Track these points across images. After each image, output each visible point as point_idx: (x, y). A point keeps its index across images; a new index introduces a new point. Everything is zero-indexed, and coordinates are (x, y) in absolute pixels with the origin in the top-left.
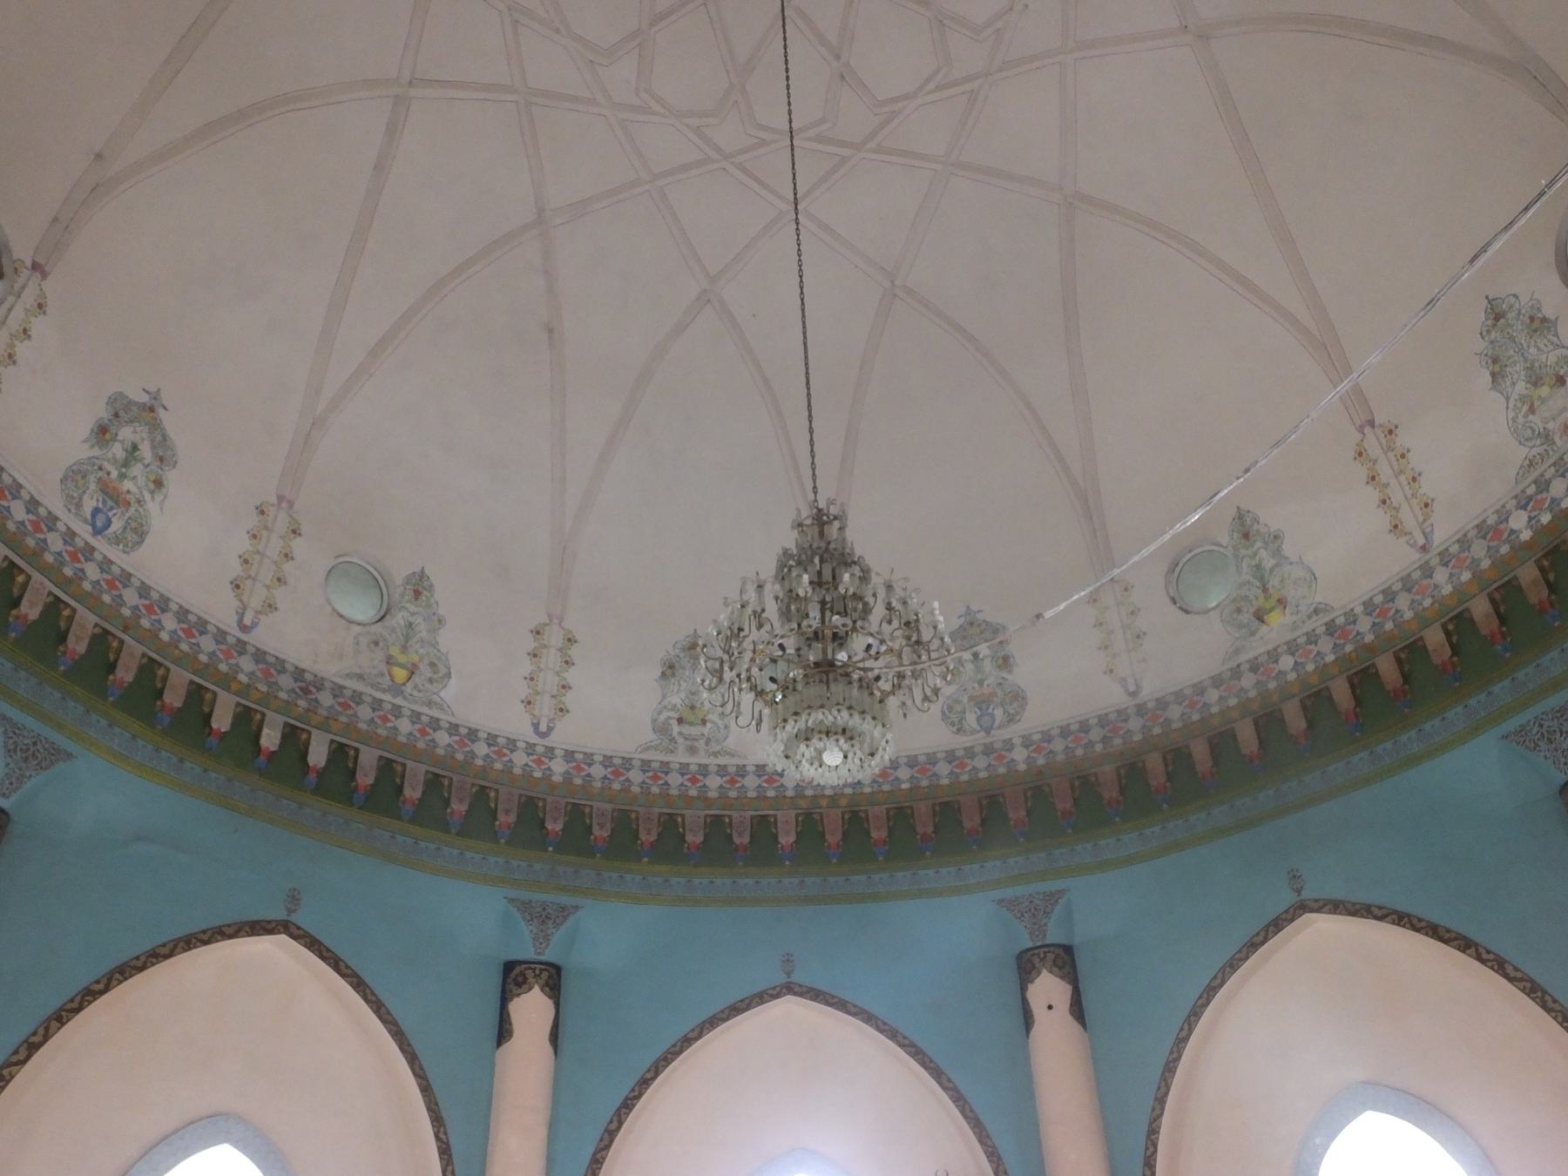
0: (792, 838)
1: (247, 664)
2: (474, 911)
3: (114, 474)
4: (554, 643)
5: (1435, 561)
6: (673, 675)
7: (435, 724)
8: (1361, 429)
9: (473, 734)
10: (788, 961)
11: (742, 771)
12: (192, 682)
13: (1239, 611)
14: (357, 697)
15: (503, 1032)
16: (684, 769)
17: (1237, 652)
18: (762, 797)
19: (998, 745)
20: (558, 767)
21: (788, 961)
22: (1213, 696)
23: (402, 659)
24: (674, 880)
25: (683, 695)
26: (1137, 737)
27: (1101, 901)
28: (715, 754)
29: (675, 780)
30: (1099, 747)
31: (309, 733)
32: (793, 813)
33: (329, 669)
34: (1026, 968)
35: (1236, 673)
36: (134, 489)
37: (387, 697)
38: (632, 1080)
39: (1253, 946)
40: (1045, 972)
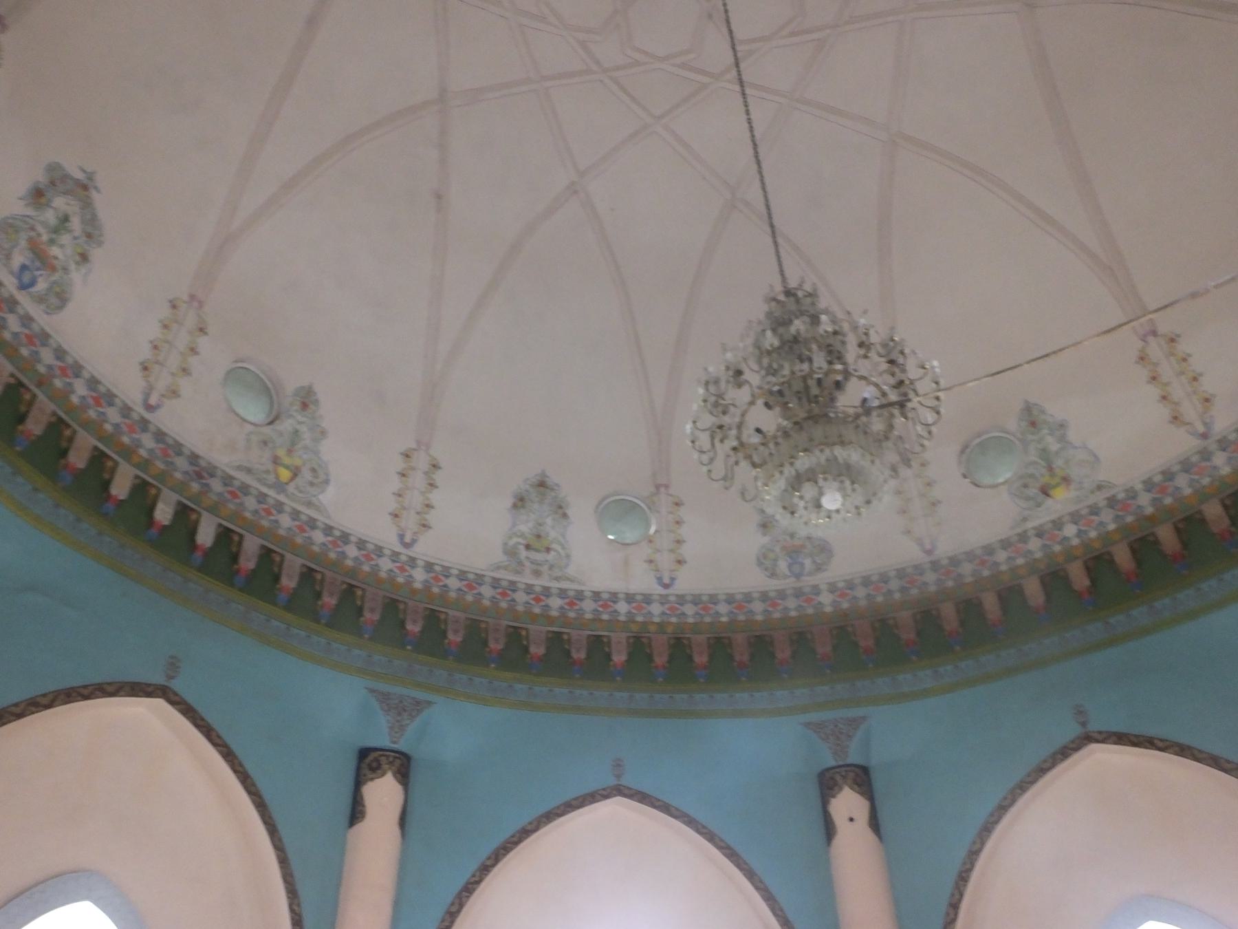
0: (624, 657)
1: (148, 441)
2: (338, 700)
3: (45, 238)
4: (420, 467)
5: (1213, 447)
6: (523, 507)
7: (312, 523)
8: (1144, 339)
9: (345, 538)
10: (618, 765)
11: (580, 596)
12: (96, 448)
13: (1026, 486)
14: (245, 489)
15: (356, 813)
16: (529, 589)
17: (1025, 519)
18: (596, 620)
19: (807, 590)
20: (419, 576)
21: (618, 765)
22: (1001, 556)
23: (287, 460)
24: (518, 686)
25: (531, 525)
26: (933, 588)
27: (900, 727)
28: (557, 579)
29: (521, 597)
30: (897, 596)
31: (199, 514)
32: (624, 635)
33: (223, 460)
34: (827, 785)
35: (1023, 537)
36: (61, 256)
37: (271, 493)
38: (473, 866)
39: (1042, 770)
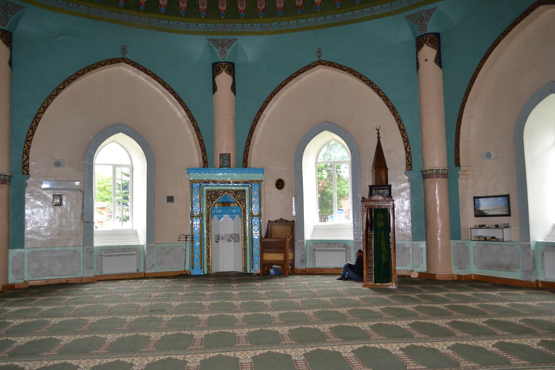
10: (319, 51)
24: (273, 24)
40: (425, 46)
